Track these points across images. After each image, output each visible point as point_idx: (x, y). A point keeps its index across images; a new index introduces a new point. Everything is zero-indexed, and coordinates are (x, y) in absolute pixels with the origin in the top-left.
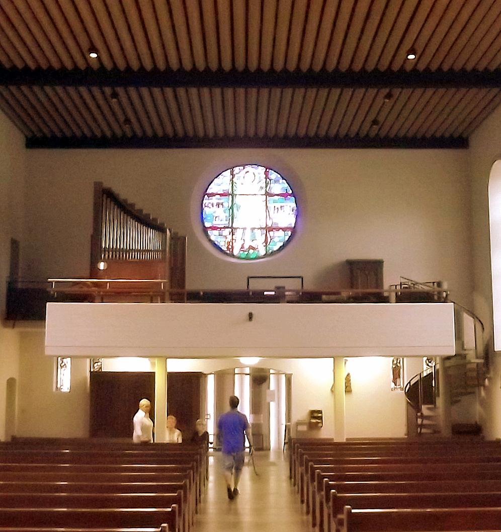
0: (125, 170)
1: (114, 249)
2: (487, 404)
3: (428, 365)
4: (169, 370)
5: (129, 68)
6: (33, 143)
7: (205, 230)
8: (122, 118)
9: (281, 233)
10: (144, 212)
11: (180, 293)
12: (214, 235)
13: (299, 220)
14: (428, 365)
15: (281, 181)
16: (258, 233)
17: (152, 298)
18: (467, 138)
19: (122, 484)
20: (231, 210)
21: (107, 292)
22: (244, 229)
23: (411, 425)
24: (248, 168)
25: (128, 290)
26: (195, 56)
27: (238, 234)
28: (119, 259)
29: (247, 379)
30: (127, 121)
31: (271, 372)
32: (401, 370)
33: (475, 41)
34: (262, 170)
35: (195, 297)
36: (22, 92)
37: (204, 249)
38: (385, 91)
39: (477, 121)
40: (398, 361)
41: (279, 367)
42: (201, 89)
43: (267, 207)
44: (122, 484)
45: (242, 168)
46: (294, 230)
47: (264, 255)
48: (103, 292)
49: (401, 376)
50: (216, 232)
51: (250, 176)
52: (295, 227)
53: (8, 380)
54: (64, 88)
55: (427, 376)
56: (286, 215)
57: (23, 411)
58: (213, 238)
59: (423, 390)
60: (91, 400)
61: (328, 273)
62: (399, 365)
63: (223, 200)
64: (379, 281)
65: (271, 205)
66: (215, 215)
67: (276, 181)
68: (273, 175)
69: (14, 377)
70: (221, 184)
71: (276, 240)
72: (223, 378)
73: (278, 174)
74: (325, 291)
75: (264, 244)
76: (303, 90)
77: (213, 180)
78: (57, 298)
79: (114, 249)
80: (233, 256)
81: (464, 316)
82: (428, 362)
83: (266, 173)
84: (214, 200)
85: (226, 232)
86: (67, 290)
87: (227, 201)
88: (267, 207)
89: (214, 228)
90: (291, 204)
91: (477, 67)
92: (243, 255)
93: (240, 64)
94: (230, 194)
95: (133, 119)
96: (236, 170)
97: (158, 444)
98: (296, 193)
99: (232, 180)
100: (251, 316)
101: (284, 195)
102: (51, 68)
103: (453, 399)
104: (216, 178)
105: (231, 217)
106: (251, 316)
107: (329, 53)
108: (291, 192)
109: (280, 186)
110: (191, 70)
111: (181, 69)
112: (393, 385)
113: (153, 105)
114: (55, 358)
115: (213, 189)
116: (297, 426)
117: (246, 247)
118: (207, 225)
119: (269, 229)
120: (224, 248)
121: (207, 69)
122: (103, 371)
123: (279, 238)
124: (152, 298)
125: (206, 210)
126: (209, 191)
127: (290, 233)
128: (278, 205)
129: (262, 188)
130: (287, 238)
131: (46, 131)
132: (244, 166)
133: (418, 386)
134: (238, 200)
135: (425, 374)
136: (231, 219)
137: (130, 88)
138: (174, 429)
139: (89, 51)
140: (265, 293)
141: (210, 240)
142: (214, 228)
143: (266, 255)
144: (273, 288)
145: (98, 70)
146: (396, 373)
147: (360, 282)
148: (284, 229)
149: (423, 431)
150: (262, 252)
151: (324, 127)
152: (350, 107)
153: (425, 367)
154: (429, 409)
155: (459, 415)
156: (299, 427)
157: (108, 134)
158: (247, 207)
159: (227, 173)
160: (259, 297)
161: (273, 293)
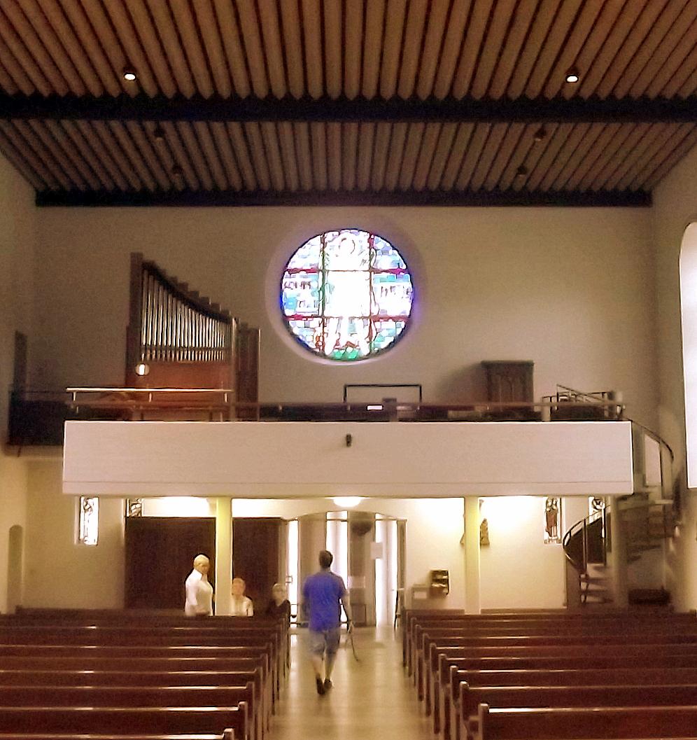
0: (174, 236)
1: (159, 347)
3: (595, 508)
4: (235, 515)
5: (179, 95)
6: (46, 198)
7: (285, 319)
8: (169, 165)
9: (391, 324)
10: (201, 295)
11: (251, 408)
12: (297, 327)
13: (416, 305)
14: (595, 508)
15: (391, 251)
16: (359, 324)
17: (211, 414)
18: (650, 192)
19: (170, 673)
20: (321, 292)
22: (340, 318)
23: (572, 591)
24: (345, 234)
25: (178, 403)
26: (271, 78)
27: (332, 325)
28: (166, 360)
29: (344, 528)
30: (177, 168)
31: (377, 518)
32: (559, 515)
33: (661, 57)
34: (364, 236)
35: (272, 413)
36: (31, 127)
37: (284, 346)
38: (536, 127)
40: (554, 503)
41: (388, 510)
42: (280, 124)
43: (371, 288)
44: (170, 673)
45: (337, 233)
46: (409, 320)
47: (367, 355)
49: (558, 523)
50: (301, 323)
51: (347, 245)
52: (410, 315)
53: (11, 529)
54: (89, 122)
55: (594, 522)
56: (397, 299)
57: (32, 572)
58: (296, 331)
59: (588, 543)
60: (127, 557)
61: (457, 380)
62: (554, 507)
63: (311, 278)
64: (527, 391)
65: (377, 286)
66: (299, 299)
67: (384, 252)
68: (380, 244)
69: (20, 524)
70: (307, 256)
71: (384, 333)
72: (310, 526)
73: (387, 241)
74: (452, 404)
75: (368, 340)
76: (421, 125)
77: (297, 251)
78: (79, 415)
79: (159, 347)
80: (324, 356)
81: (646, 439)
82: (595, 504)
83: (370, 241)
84: (298, 278)
85: (315, 323)
86: (94, 403)
87: (315, 280)
88: (371, 288)
89: (297, 317)
90: (405, 284)
91: (664, 93)
92: (339, 355)
93: (334, 89)
94: (320, 270)
95: (185, 166)
96: (329, 236)
97: (219, 618)
98: (412, 268)
99: (323, 250)
100: (349, 440)
101: (396, 272)
102: (70, 94)
103: (630, 556)
104: (301, 247)
105: (321, 302)
106: (349, 440)
107: (458, 74)
108: (404, 267)
109: (390, 259)
110: (266, 97)
111: (252, 96)
112: (546, 535)
113: (212, 146)
114: (76, 497)
115: (296, 263)
116: (414, 592)
117: (343, 343)
118: (288, 312)
119: (374, 319)
120: (312, 345)
121: (289, 96)
122: (143, 515)
123: (388, 332)
124: (211, 414)
125: (287, 292)
126: (291, 266)
127: (403, 324)
128: (387, 285)
129: (364, 261)
130: (399, 331)
131: (64, 182)
132: (339, 230)
133: (581, 536)
134: (330, 278)
135: (591, 520)
136: (321, 305)
137: (181, 123)
138: (242, 596)
139: (124, 71)
140: (369, 408)
141: (292, 334)
142: (297, 317)
143: (369, 355)
144: (379, 401)
146: (552, 519)
147: (501, 392)
148: (395, 319)
149: (589, 599)
150: (365, 350)
151: (451, 177)
152: (488, 149)
153: (591, 510)
154: (596, 568)
155: (638, 578)
156: (415, 593)
157: (151, 186)
158: (344, 288)
159: (316, 241)
160: (360, 414)
161: (380, 408)
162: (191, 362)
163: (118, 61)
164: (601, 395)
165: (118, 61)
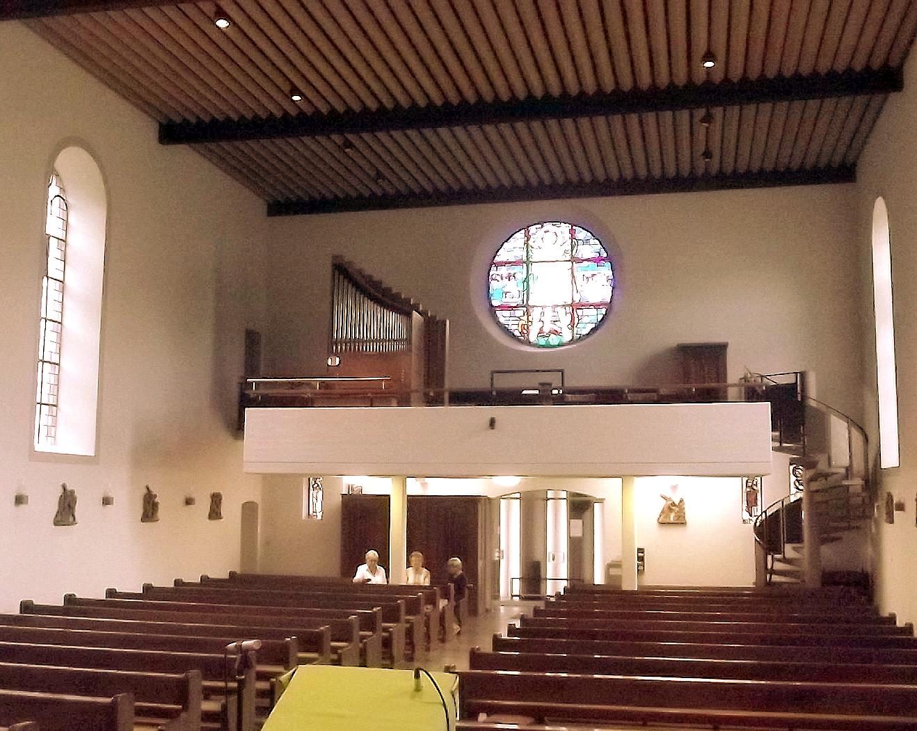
0: (373, 240)
1: (352, 341)
2: (876, 542)
3: (797, 488)
4: (408, 493)
5: (447, 103)
6: (278, 208)
7: (492, 310)
8: (373, 174)
9: (593, 311)
10: (394, 291)
11: (436, 390)
12: (503, 316)
13: (616, 292)
14: (797, 488)
15: (593, 241)
16: (561, 311)
17: (372, 400)
18: (854, 165)
19: (636, 658)
20: (525, 283)
21: (317, 394)
22: (543, 307)
23: (763, 569)
24: (548, 226)
25: (354, 391)
26: (423, 88)
27: (535, 314)
28: (353, 350)
29: (564, 506)
30: (379, 175)
31: (549, 497)
32: (759, 495)
33: (796, 37)
34: (565, 228)
35: (461, 398)
36: (379, 140)
37: (488, 336)
38: (701, 112)
39: (860, 135)
40: (755, 483)
41: (605, 490)
42: (562, 121)
43: (573, 277)
44: (636, 658)
45: (540, 226)
46: (609, 306)
47: (570, 341)
48: (312, 393)
49: (759, 503)
50: (507, 313)
51: (549, 237)
52: (611, 302)
53: (243, 505)
54: (480, 127)
55: (795, 501)
56: (598, 286)
57: (267, 543)
58: (502, 320)
59: (787, 526)
60: (343, 533)
61: (654, 362)
62: (755, 487)
63: (516, 269)
64: (721, 374)
65: (578, 275)
66: (506, 290)
67: (586, 242)
68: (581, 234)
69: (252, 499)
70: (512, 249)
71: (585, 320)
72: (532, 506)
73: (588, 231)
74: (650, 387)
75: (570, 326)
76: (736, 108)
77: (503, 245)
78: (260, 403)
79: (352, 341)
80: (529, 343)
81: (832, 419)
82: (797, 484)
83: (572, 232)
84: (504, 271)
85: (519, 313)
86: (271, 392)
87: (520, 272)
88: (573, 277)
89: (502, 308)
90: (606, 271)
91: (835, 67)
92: (542, 341)
93: (645, 81)
94: (524, 262)
95: (386, 173)
96: (532, 229)
97: (394, 587)
98: (612, 257)
99: (526, 243)
100: (492, 423)
101: (598, 260)
102: (349, 110)
103: (825, 535)
104: (506, 241)
105: (525, 292)
106: (492, 423)
107: (525, 72)
108: (605, 255)
109: (591, 249)
110: (560, 96)
111: (547, 95)
112: (746, 516)
113: (401, 151)
114: (304, 479)
115: (503, 256)
116: (609, 569)
118: (495, 303)
119: (576, 307)
120: (517, 333)
121: (600, 90)
122: (363, 493)
123: (590, 318)
124: (372, 400)
125: (493, 284)
126: (497, 259)
127: (604, 311)
128: (588, 274)
129: (565, 252)
130: (600, 317)
131: (464, 180)
132: (542, 223)
133: (778, 514)
134: (535, 268)
135: (793, 499)
136: (525, 295)
137: (550, 122)
138: (421, 568)
139: (704, 60)
140: (524, 392)
141: (498, 323)
142: (502, 308)
143: (572, 342)
144: (537, 386)
145: (653, 111)
146: (751, 499)
147: (696, 374)
148: (597, 306)
149: (775, 578)
150: (567, 336)
151: (729, 160)
152: (669, 137)
153: (793, 490)
154: (794, 549)
155: (830, 555)
156: (610, 569)
157: (481, 185)
158: (548, 277)
159: (520, 236)
160: (514, 398)
161: (537, 392)
162: (373, 353)
163: (701, 46)
164: (57, 373)
165: (701, 46)
